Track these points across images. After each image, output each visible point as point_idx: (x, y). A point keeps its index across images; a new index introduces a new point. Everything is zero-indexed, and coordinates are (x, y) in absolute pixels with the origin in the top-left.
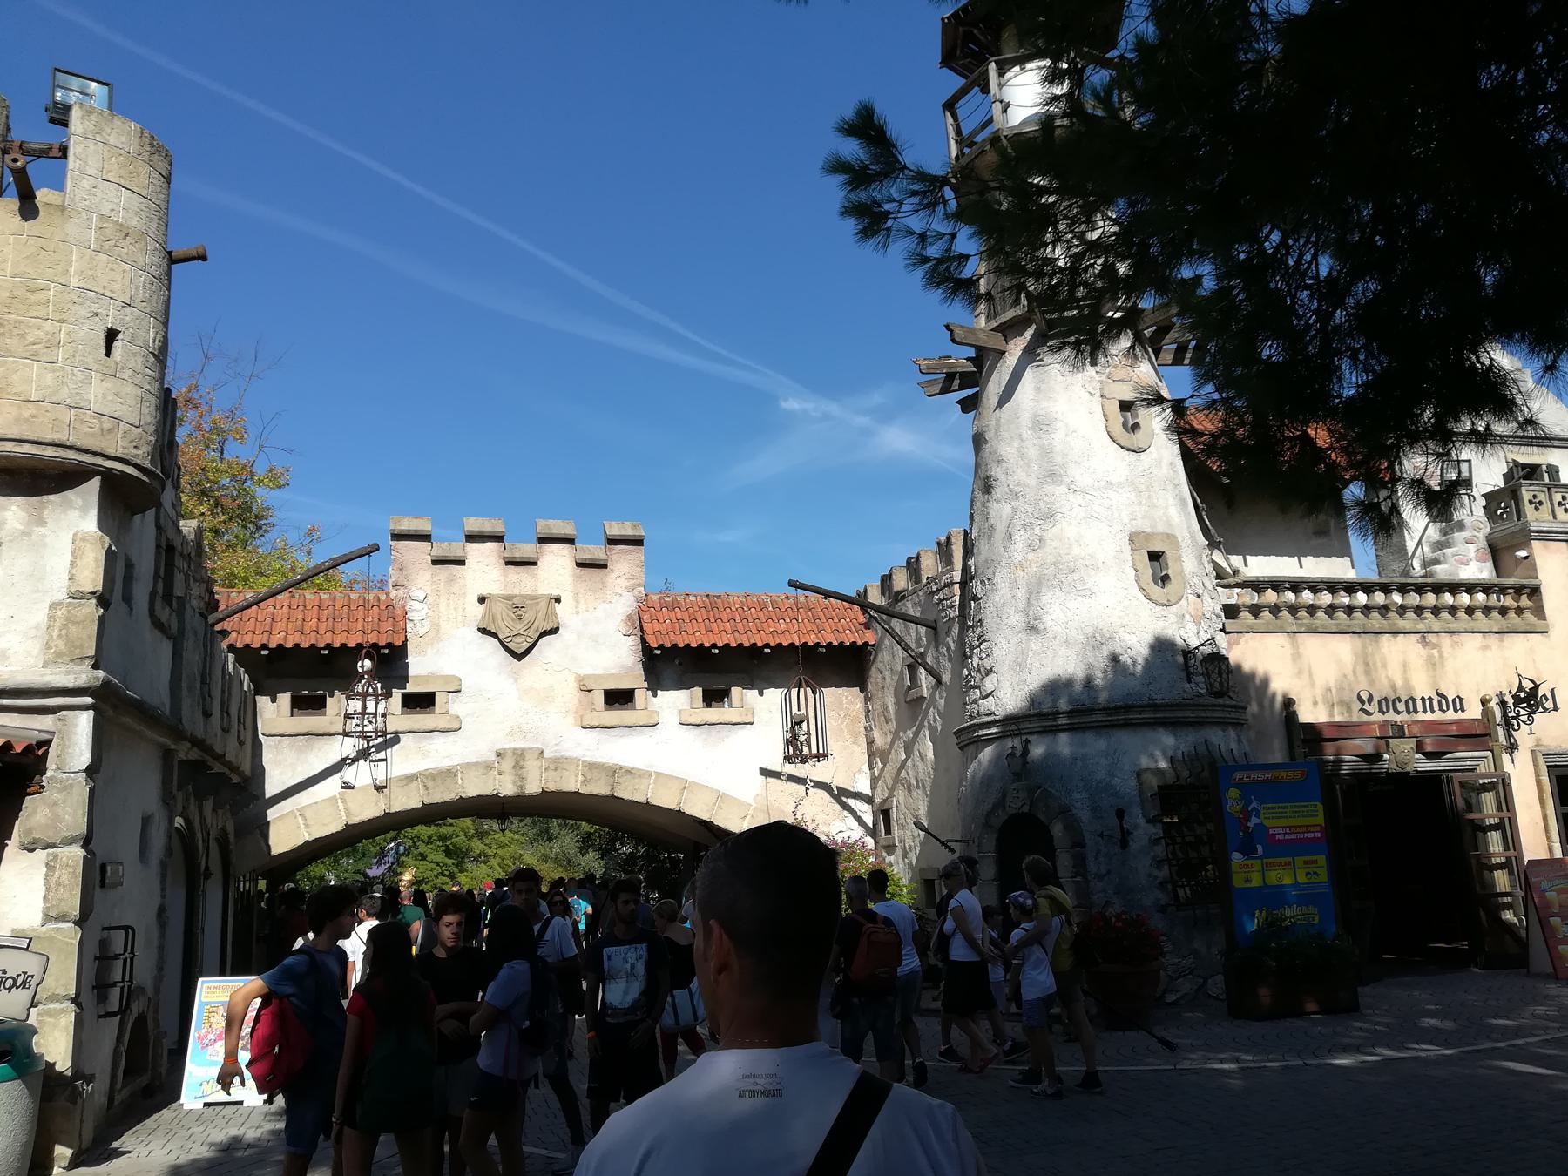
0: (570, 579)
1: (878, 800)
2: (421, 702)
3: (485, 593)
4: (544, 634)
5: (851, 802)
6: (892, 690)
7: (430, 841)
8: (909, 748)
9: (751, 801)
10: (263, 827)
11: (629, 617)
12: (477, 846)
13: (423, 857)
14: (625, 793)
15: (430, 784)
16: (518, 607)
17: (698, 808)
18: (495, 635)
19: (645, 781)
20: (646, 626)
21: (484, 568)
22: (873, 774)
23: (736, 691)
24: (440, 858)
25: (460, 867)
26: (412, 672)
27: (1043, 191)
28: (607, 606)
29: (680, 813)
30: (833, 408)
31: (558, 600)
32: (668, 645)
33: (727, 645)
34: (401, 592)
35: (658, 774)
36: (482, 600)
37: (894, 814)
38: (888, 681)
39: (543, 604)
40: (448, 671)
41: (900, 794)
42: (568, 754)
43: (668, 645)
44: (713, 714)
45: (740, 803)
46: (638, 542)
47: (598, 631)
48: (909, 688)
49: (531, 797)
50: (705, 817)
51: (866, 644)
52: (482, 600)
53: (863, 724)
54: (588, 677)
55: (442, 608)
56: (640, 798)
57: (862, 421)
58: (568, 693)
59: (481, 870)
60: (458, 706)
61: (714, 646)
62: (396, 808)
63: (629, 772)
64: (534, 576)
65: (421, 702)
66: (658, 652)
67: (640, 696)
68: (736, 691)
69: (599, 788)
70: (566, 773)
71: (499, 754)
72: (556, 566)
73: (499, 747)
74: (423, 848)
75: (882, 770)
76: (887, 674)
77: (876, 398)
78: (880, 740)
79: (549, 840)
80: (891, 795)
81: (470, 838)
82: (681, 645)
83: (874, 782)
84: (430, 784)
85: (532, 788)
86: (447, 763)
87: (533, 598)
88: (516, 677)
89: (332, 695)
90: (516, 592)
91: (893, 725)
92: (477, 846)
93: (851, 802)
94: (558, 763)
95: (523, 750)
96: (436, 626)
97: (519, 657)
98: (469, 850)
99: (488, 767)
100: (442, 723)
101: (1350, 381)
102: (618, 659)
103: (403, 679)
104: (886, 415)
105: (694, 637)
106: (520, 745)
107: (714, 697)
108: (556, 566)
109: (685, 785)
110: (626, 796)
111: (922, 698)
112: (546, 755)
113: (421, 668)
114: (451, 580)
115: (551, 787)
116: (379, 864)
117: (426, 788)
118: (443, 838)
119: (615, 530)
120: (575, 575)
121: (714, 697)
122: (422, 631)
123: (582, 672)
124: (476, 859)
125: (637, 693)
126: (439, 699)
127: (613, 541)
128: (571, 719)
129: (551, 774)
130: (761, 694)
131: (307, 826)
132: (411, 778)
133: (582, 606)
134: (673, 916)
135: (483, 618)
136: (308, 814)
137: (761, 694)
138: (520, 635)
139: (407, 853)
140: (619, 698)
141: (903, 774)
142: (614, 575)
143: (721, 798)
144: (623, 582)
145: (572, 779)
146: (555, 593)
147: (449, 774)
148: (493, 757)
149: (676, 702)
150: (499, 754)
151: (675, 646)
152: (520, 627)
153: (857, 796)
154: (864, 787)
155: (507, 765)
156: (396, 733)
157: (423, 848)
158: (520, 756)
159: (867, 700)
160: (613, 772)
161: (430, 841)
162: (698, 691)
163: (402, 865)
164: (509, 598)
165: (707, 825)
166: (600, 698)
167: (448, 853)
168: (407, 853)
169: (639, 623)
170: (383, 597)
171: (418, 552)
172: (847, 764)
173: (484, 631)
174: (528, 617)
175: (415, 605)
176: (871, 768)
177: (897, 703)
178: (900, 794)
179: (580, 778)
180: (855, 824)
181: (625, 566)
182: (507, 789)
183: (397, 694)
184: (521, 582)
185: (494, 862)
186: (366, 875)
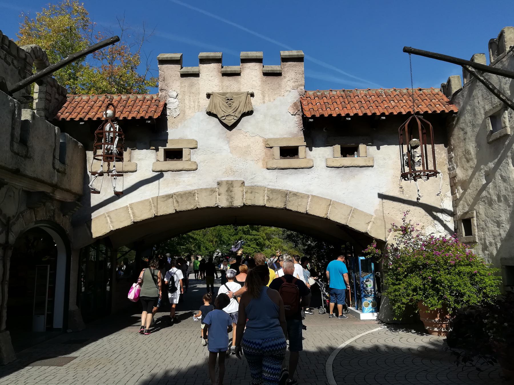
0: (259, 83)
1: (459, 213)
2: (175, 155)
3: (210, 92)
4: (244, 115)
5: (439, 215)
6: (473, 139)
8: (489, 176)
9: (373, 214)
10: (89, 221)
11: (295, 104)
12: (267, 243)
13: (249, 246)
14: (293, 206)
15: (180, 200)
16: (229, 100)
17: (338, 217)
18: (215, 116)
19: (305, 200)
20: (304, 107)
21: (210, 77)
23: (362, 147)
24: (255, 246)
25: (262, 250)
26: (170, 137)
28: (281, 98)
29: (327, 220)
31: (252, 95)
32: (318, 115)
33: (356, 114)
34: (164, 93)
35: (313, 196)
36: (209, 96)
37: (475, 222)
38: (469, 134)
39: (243, 98)
40: (190, 137)
41: (481, 208)
42: (259, 184)
43: (318, 115)
44: (348, 161)
45: (366, 215)
46: (299, 59)
47: (277, 108)
48: (492, 132)
49: (236, 208)
50: (343, 222)
51: (452, 112)
52: (209, 96)
53: (447, 166)
54: (271, 139)
55: (187, 102)
56: (302, 210)
58: (259, 149)
60: (196, 157)
61: (348, 115)
62: (160, 213)
63: (295, 194)
64: (238, 82)
65: (175, 155)
66: (311, 120)
67: (302, 151)
68: (362, 147)
69: (278, 204)
70: (257, 195)
71: (219, 184)
72: (251, 76)
73: (219, 179)
74: (249, 243)
75: (463, 194)
76: (469, 130)
78: (460, 174)
80: (472, 208)
81: (264, 240)
82: (326, 115)
83: (456, 202)
84: (180, 200)
85: (238, 203)
86: (190, 188)
87: (237, 94)
88: (228, 140)
89: (126, 151)
90: (229, 91)
91: (474, 162)
92: (267, 243)
93: (439, 215)
94: (253, 189)
95: (232, 181)
96: (183, 112)
97: (230, 128)
98: (264, 245)
99: (213, 191)
100: (187, 166)
101: (343, 246)
102: (288, 128)
103: (164, 141)
105: (335, 110)
106: (231, 179)
107: (348, 151)
108: (251, 76)
109: (330, 203)
110: (293, 208)
111: (507, 136)
112: (246, 184)
113: (176, 134)
114: (191, 85)
115: (249, 203)
117: (177, 202)
118: (255, 240)
119: (285, 53)
120: (263, 82)
121: (348, 151)
122: (175, 115)
123: (267, 137)
124: (267, 247)
125: (300, 149)
126: (185, 153)
127: (285, 60)
128: (260, 164)
129: (249, 195)
130: (378, 149)
131: (112, 222)
132: (170, 196)
133: (267, 99)
135: (209, 106)
136: (112, 215)
137: (378, 149)
138: (231, 117)
140: (289, 152)
141: (484, 193)
142: (286, 80)
143: (353, 211)
144: (291, 84)
145: (261, 198)
146: (250, 91)
147: (191, 194)
148: (216, 185)
149: (323, 155)
150: (219, 184)
151: (322, 116)
152: (230, 111)
153: (443, 211)
154: (448, 205)
155: (223, 189)
156: (162, 171)
157: (249, 243)
158: (230, 185)
159: (449, 152)
160: (286, 194)
161: (251, 240)
162: (338, 147)
164: (224, 94)
165: (345, 228)
166: (277, 152)
167: (257, 244)
169: (300, 107)
170: (155, 97)
171: (174, 70)
172: (436, 190)
173: (210, 114)
174: (235, 105)
175: (171, 100)
176: (453, 193)
177: (479, 145)
178: (481, 208)
179: (266, 198)
180: (441, 228)
181: (293, 76)
182: (223, 203)
183: (161, 149)
184: (231, 85)
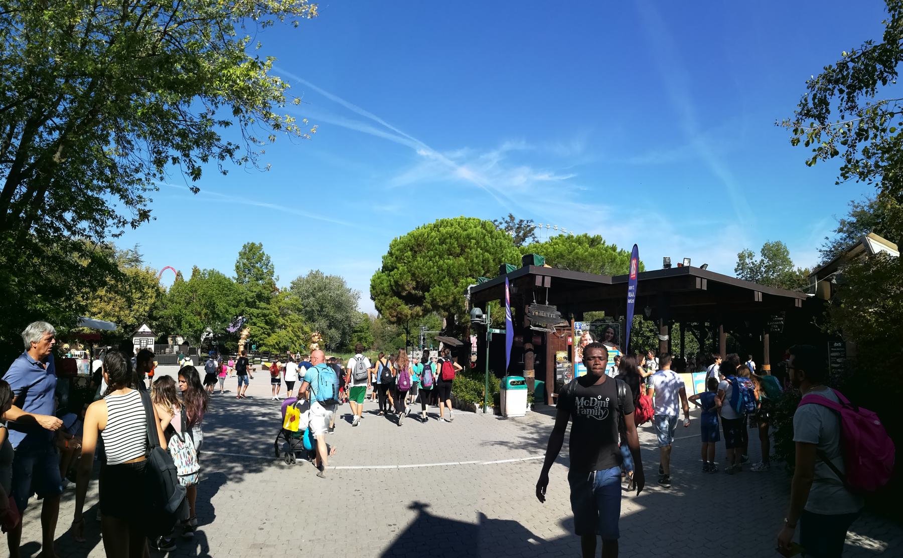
7: (258, 316)
12: (281, 320)
13: (255, 324)
22: (637, 258)
24: (263, 325)
27: (49, 520)
30: (440, 156)
57: (451, 163)
59: (283, 332)
74: (254, 320)
77: (459, 154)
79: (313, 321)
81: (278, 316)
92: (281, 320)
98: (277, 323)
104: (461, 162)
116: (234, 326)
124: (280, 327)
134: (708, 340)
139: (247, 322)
157: (254, 320)
161: (258, 316)
163: (245, 327)
167: (267, 323)
168: (247, 322)
185: (289, 329)
186: (226, 331)
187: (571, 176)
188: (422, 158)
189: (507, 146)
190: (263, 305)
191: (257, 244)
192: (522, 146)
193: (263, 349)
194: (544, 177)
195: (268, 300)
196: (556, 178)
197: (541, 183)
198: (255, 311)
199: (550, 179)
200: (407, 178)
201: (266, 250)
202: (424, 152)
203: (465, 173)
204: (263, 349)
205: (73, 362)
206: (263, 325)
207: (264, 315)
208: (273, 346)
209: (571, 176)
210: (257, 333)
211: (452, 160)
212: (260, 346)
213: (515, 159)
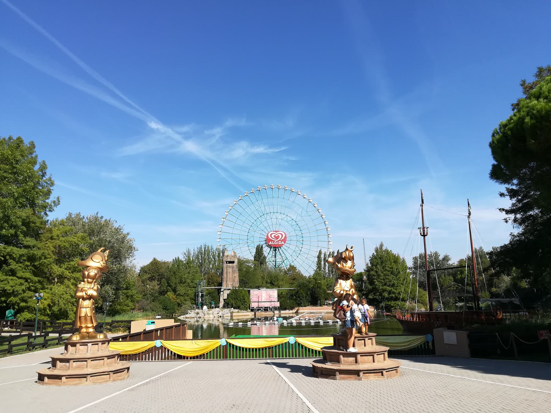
12: (57, 269)
24: (28, 275)
30: (169, 131)
57: (178, 137)
77: (186, 129)
92: (57, 269)
104: (187, 136)
187: (283, 148)
188: (153, 131)
189: (230, 123)
190: (29, 241)
191: (27, 142)
192: (243, 123)
193: (26, 315)
194: (260, 150)
195: (37, 236)
196: (270, 151)
197: (257, 156)
198: (17, 251)
199: (265, 151)
200: (137, 148)
201: (42, 154)
202: (154, 125)
203: (191, 147)
204: (26, 315)
205: (340, 325)
206: (28, 275)
207: (32, 259)
208: (43, 311)
209: (283, 148)
210: (19, 289)
211: (180, 133)
212: (20, 311)
213: (236, 135)
